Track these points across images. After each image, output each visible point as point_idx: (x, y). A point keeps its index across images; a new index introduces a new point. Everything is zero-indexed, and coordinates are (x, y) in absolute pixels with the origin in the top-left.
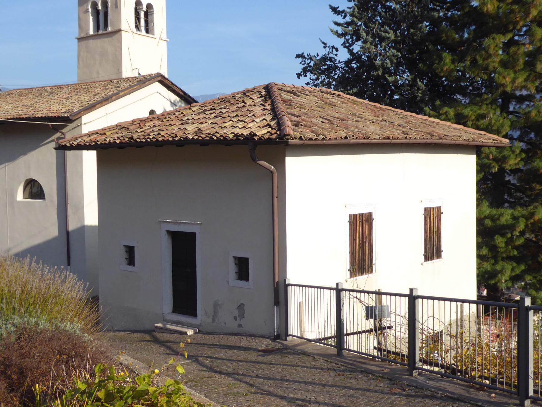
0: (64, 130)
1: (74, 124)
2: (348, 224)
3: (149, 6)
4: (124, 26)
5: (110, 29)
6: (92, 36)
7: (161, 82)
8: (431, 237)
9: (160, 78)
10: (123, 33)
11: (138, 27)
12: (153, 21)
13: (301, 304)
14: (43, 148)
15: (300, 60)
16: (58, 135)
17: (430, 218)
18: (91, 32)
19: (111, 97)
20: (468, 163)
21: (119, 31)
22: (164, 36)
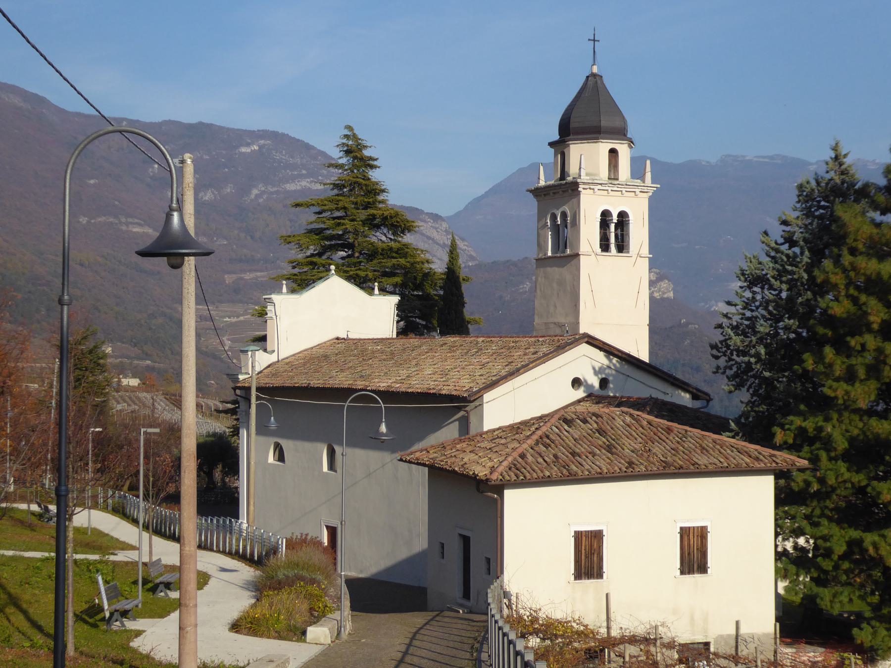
0: (467, 409)
1: (477, 403)
2: (573, 539)
3: (623, 215)
4: (584, 248)
5: (568, 251)
6: (550, 258)
7: (588, 343)
8: (689, 554)
9: (586, 340)
10: (582, 259)
11: (605, 247)
12: (628, 235)
13: (607, 595)
14: (444, 430)
15: (720, 330)
16: (462, 413)
17: (689, 536)
18: (550, 254)
19: (518, 370)
20: (763, 488)
21: (577, 255)
22: (645, 251)
